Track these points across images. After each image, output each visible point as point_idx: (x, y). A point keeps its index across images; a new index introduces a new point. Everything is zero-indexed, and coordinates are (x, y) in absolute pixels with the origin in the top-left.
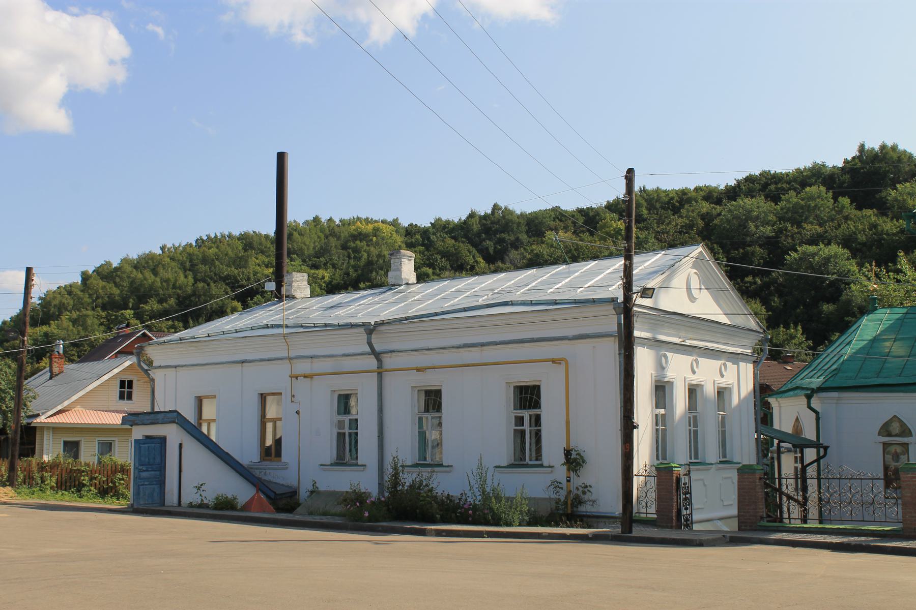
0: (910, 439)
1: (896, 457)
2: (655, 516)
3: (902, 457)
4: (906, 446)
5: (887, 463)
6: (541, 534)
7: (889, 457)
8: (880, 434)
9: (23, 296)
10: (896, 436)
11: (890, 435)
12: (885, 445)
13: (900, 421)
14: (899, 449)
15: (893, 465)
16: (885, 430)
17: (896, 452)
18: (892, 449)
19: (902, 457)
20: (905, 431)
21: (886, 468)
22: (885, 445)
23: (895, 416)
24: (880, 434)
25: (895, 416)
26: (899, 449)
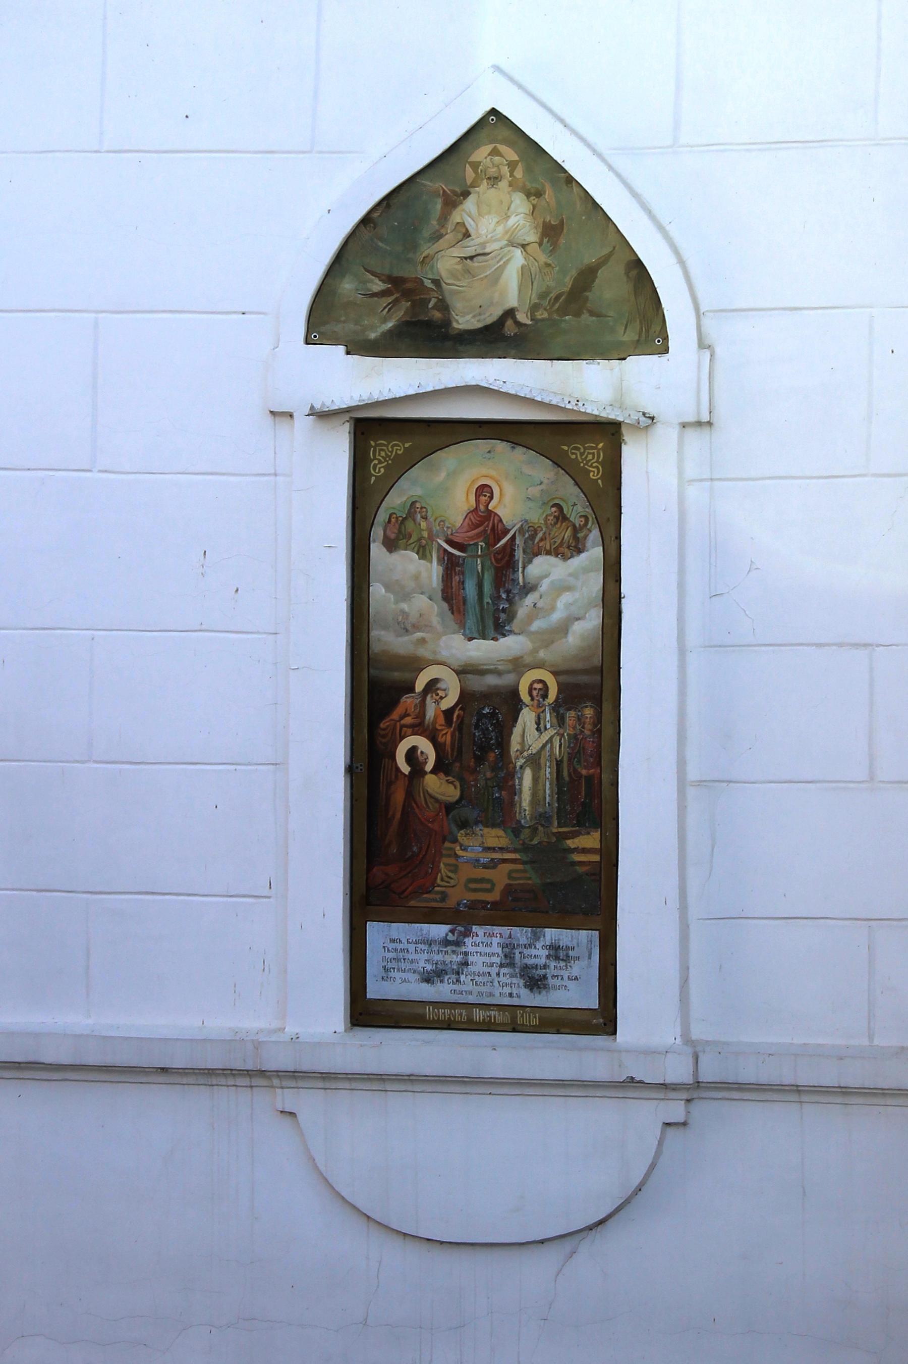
0: (639, 368)
1: (486, 570)
2: (596, 858)
3: (544, 569)
4: (586, 449)
5: (385, 639)
6: (584, 862)
7: (409, 575)
8: (325, 320)
9: (626, 588)
10: (496, 338)
11: (426, 331)
12: (380, 440)
13: (541, 172)
14: (519, 488)
15: (451, 655)
16: (387, 278)
17: (484, 521)
18: (449, 487)
19: (544, 569)
20: (602, 295)
21: (377, 693)
22: (371, 430)
23: (494, 122)
24: (325, 320)
25: (494, 122)
26: (519, 488)
